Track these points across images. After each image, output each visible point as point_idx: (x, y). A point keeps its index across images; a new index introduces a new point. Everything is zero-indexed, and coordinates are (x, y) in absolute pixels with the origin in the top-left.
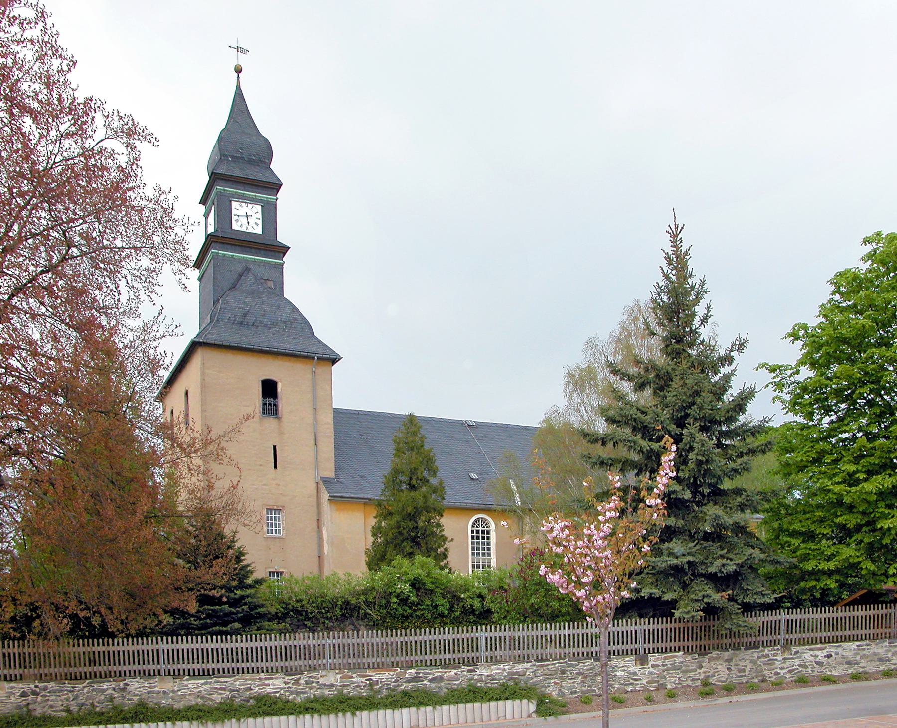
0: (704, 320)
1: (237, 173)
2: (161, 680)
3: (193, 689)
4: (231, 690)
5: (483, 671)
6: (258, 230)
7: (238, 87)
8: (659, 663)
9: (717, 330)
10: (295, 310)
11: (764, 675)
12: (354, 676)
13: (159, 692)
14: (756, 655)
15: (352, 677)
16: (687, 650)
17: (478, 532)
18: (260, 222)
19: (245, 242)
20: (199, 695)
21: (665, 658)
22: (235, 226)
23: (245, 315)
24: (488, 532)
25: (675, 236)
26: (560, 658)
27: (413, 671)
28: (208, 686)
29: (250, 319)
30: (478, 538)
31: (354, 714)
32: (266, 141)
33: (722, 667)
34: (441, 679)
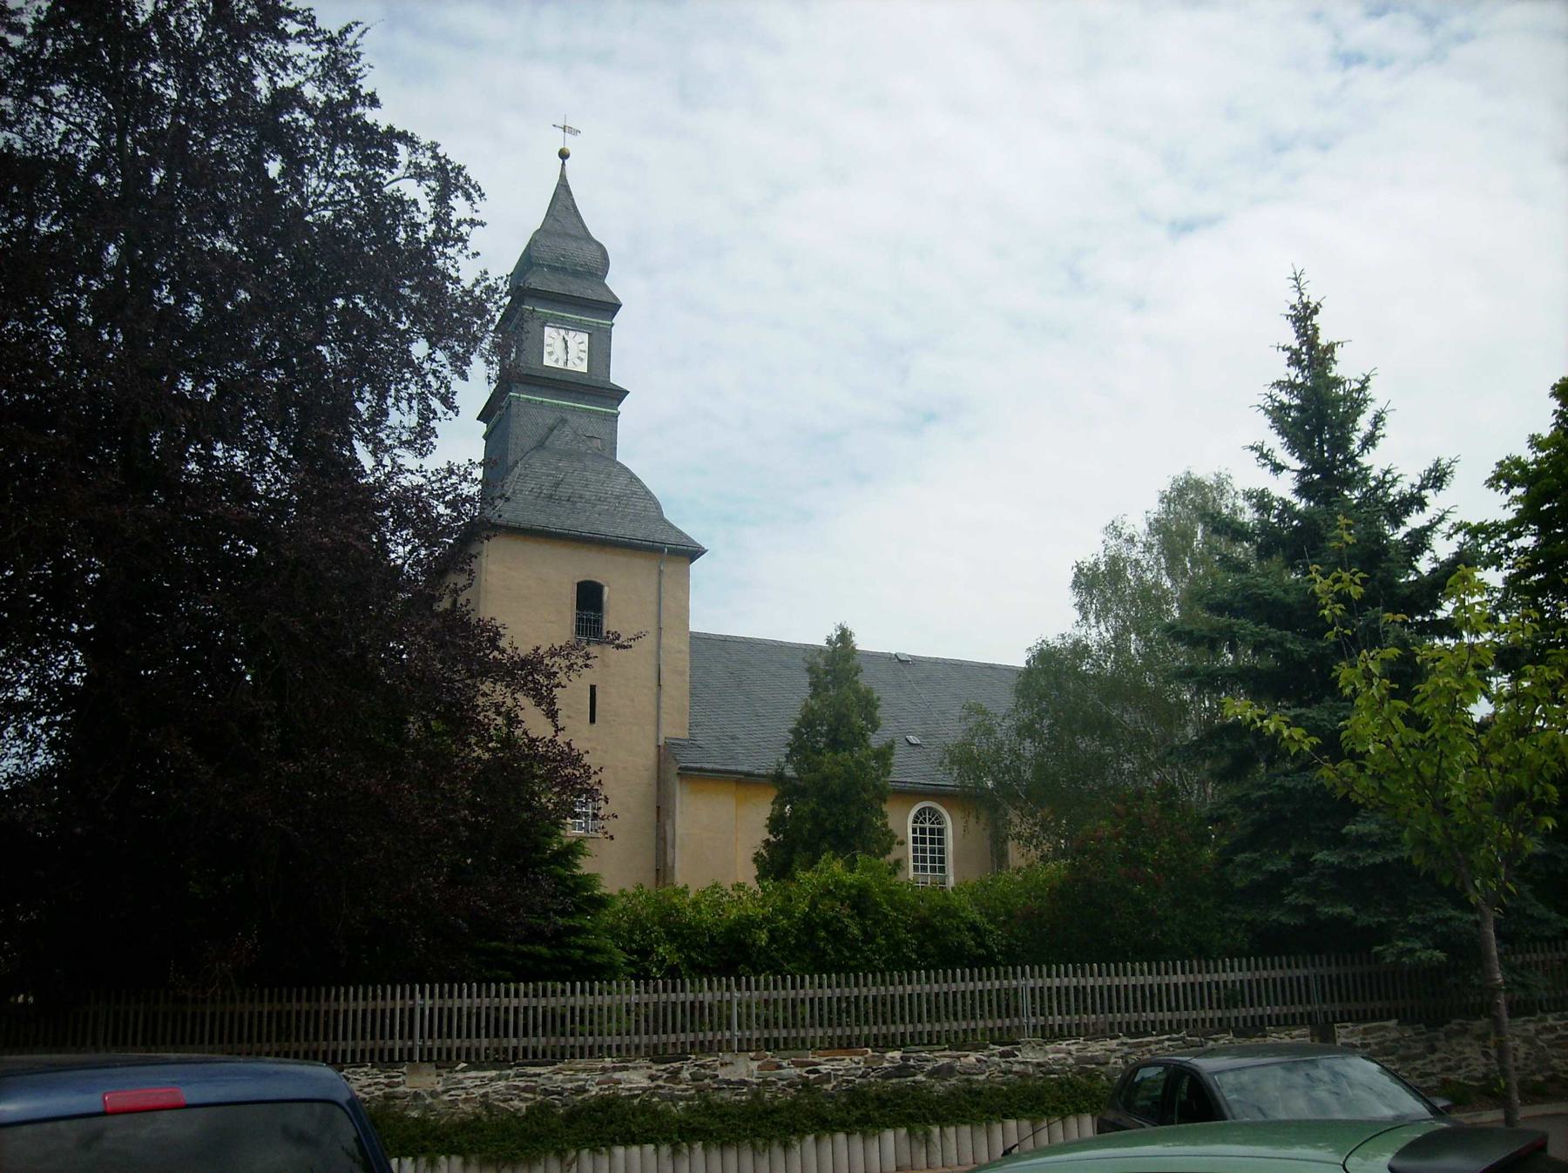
0: (1370, 441)
1: (555, 287)
2: (415, 1071)
3: (472, 1087)
4: (546, 1092)
5: (1029, 1055)
6: (583, 368)
7: (563, 177)
8: (1356, 1040)
9: (1393, 458)
10: (633, 478)
11: (1553, 1069)
12: (784, 1064)
13: (406, 1095)
14: (1531, 1027)
15: (780, 1067)
16: (1405, 1018)
17: (923, 831)
18: (585, 356)
19: (561, 383)
20: (485, 1101)
21: (1366, 1032)
22: (548, 361)
23: (557, 485)
24: (941, 832)
25: (1304, 317)
26: (1171, 1031)
27: (897, 1054)
28: (503, 1083)
29: (564, 491)
30: (923, 841)
31: (786, 1146)
32: (600, 246)
33: (1472, 1052)
34: (949, 1070)
